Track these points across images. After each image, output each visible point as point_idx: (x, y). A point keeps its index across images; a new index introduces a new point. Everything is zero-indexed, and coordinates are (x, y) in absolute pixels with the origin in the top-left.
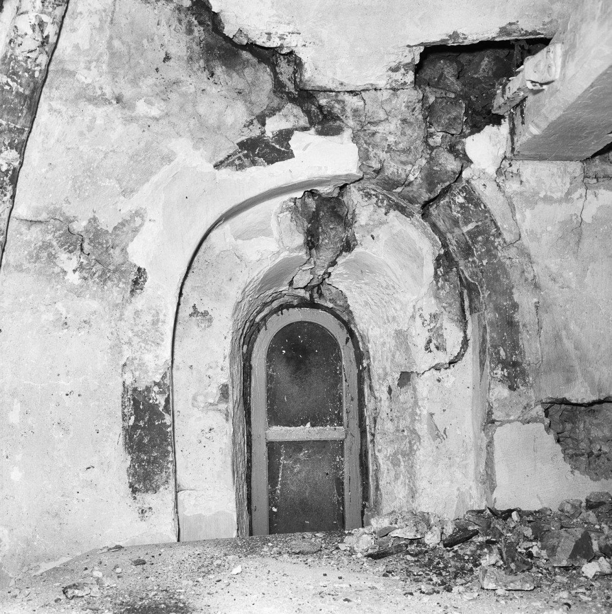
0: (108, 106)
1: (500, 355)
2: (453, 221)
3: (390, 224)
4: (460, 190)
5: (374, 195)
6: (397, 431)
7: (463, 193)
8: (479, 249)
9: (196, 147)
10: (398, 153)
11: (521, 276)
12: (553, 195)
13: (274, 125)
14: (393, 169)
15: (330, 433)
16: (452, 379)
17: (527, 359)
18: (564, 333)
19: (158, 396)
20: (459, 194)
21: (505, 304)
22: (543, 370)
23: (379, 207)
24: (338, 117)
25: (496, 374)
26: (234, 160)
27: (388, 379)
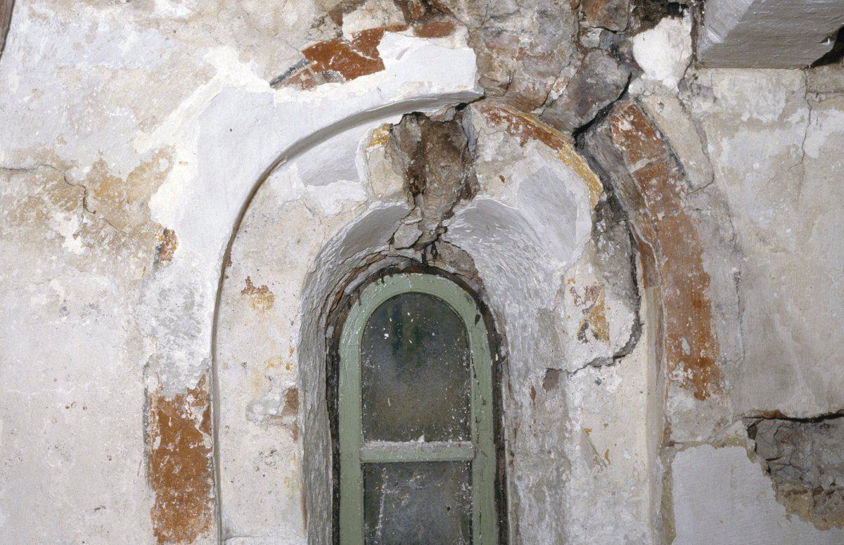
0: (117, 7)
1: (681, 349)
2: (616, 156)
3: (528, 160)
4: (625, 112)
5: (504, 118)
6: (542, 451)
7: (629, 116)
8: (651, 197)
9: (244, 59)
10: (535, 60)
11: (714, 235)
12: (761, 118)
13: (353, 25)
14: (526, 83)
15: (452, 449)
16: (618, 380)
17: (721, 354)
18: (777, 317)
19: (193, 409)
20: (624, 117)
21: (690, 275)
22: (745, 370)
23: (512, 135)
24: (447, 9)
25: (676, 376)
26: (299, 75)
27: (530, 377)
